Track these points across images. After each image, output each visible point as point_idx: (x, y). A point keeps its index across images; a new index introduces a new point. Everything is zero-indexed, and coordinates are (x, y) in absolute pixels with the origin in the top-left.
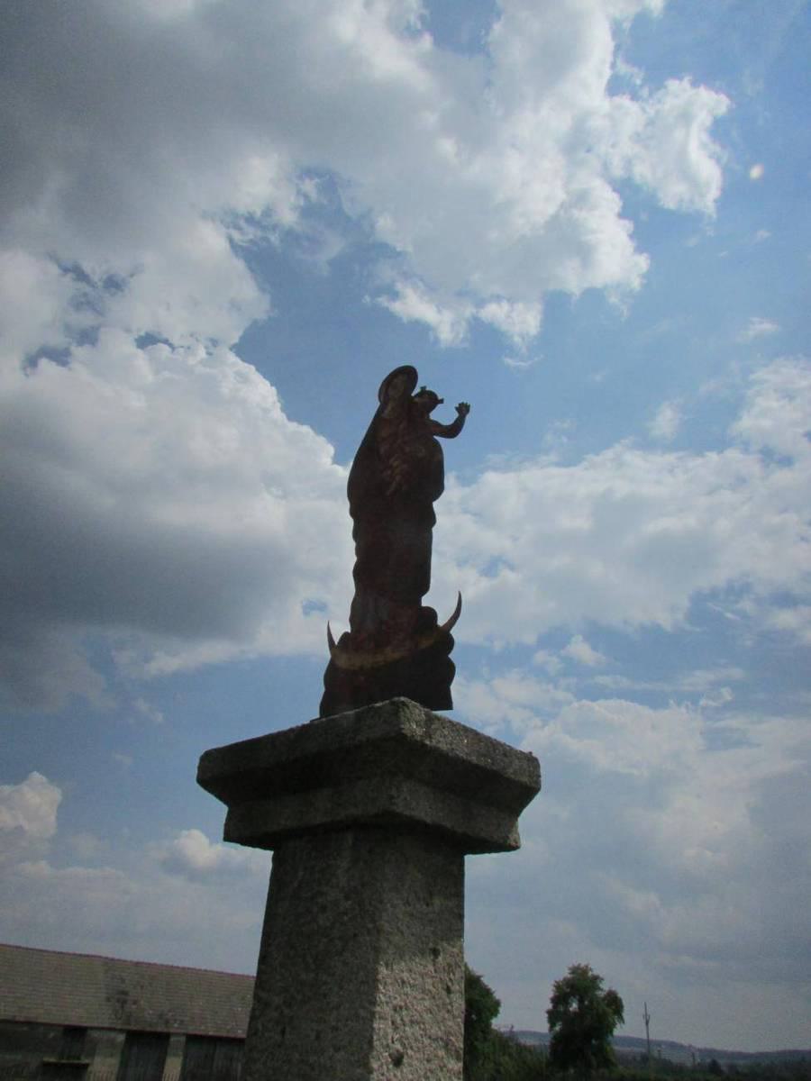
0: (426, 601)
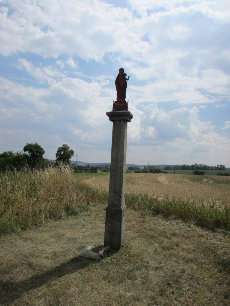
0: (125, 100)
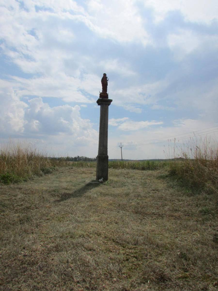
0: (107, 92)
